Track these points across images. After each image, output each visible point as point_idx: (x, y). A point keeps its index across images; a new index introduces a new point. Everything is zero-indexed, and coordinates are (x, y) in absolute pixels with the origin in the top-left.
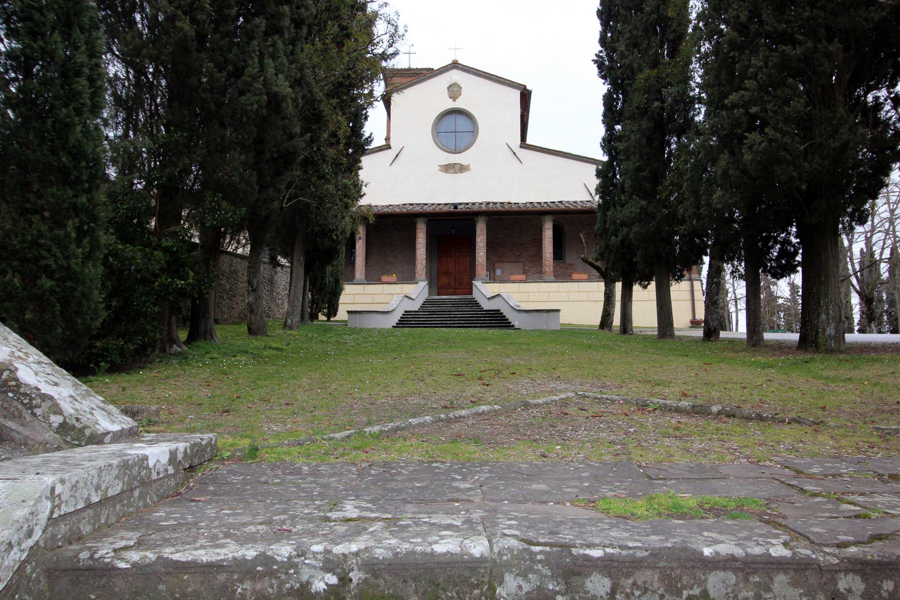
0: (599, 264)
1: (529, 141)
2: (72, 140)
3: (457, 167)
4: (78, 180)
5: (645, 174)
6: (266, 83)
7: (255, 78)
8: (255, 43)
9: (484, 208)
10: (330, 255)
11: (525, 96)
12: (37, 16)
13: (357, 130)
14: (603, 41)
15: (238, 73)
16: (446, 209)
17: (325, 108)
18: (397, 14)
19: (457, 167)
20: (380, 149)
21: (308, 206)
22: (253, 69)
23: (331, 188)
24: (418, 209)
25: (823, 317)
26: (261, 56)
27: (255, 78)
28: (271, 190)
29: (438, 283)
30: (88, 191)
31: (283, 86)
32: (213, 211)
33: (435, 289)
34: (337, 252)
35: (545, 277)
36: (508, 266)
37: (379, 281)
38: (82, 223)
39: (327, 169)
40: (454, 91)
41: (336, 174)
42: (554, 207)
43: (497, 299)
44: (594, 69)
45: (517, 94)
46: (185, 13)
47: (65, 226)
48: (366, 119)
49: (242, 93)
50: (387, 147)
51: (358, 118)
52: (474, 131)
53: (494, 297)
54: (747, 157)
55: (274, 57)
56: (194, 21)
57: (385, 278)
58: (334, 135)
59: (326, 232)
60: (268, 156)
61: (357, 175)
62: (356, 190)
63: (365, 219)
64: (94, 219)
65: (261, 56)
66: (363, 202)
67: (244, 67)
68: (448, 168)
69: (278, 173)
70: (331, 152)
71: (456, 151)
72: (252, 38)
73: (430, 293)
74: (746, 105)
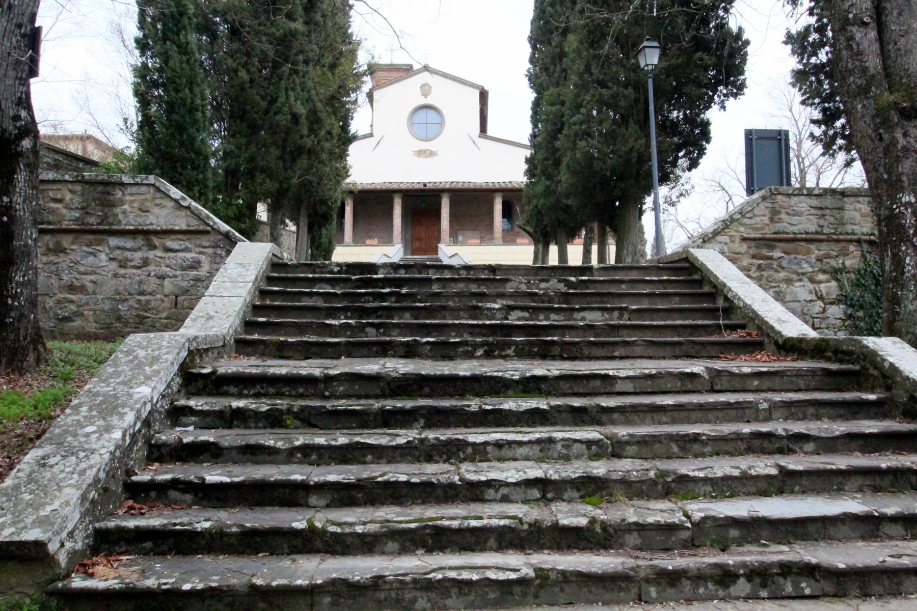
0: (528, 228)
1: (490, 131)
2: (196, 145)
3: (428, 153)
4: (199, 166)
5: (550, 162)
6: (291, 108)
7: (283, 104)
8: (283, 82)
9: (448, 186)
10: (326, 218)
11: (484, 96)
12: (178, 80)
13: (345, 128)
14: (532, 60)
15: (274, 101)
16: (417, 187)
17: (323, 115)
18: (374, 47)
19: (428, 153)
20: (365, 137)
21: (311, 182)
22: (282, 99)
23: (328, 169)
24: (395, 187)
25: (625, 251)
26: (287, 89)
27: (283, 104)
28: (290, 171)
29: (411, 245)
30: (202, 172)
31: (301, 110)
32: (261, 184)
33: (410, 252)
34: (331, 216)
35: (496, 242)
36: (468, 233)
37: (364, 244)
38: (201, 189)
39: (324, 156)
40: (425, 90)
41: (331, 160)
42: (503, 186)
43: (456, 257)
44: (526, 81)
45: (477, 93)
46: (243, 67)
47: (193, 190)
48: (352, 119)
49: (276, 114)
50: (371, 135)
51: (345, 119)
52: (442, 124)
53: (453, 256)
54: (578, 155)
55: (293, 89)
56: (248, 71)
57: (368, 242)
58: (329, 133)
59: (323, 202)
60: (288, 149)
61: (346, 160)
62: (344, 172)
63: (351, 192)
64: (206, 187)
65: (287, 89)
66: (348, 180)
67: (277, 98)
68: (420, 153)
69: (294, 161)
70: (327, 145)
71: (427, 140)
72: (281, 79)
73: (405, 254)
74: (581, 123)
